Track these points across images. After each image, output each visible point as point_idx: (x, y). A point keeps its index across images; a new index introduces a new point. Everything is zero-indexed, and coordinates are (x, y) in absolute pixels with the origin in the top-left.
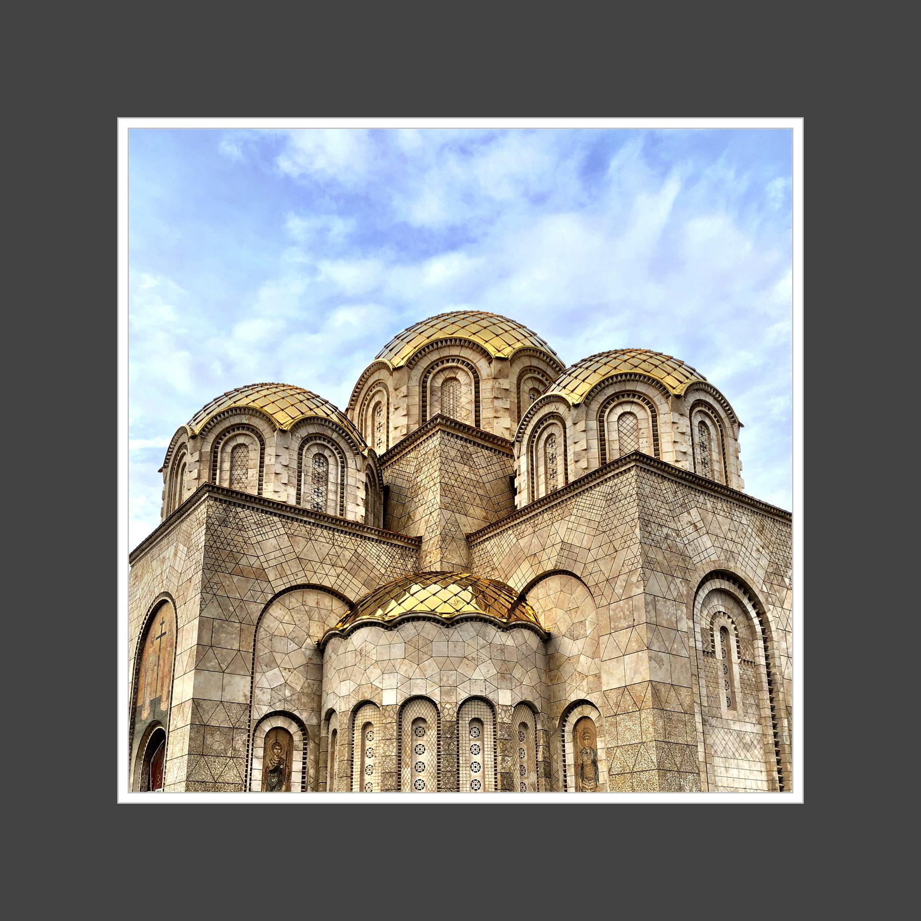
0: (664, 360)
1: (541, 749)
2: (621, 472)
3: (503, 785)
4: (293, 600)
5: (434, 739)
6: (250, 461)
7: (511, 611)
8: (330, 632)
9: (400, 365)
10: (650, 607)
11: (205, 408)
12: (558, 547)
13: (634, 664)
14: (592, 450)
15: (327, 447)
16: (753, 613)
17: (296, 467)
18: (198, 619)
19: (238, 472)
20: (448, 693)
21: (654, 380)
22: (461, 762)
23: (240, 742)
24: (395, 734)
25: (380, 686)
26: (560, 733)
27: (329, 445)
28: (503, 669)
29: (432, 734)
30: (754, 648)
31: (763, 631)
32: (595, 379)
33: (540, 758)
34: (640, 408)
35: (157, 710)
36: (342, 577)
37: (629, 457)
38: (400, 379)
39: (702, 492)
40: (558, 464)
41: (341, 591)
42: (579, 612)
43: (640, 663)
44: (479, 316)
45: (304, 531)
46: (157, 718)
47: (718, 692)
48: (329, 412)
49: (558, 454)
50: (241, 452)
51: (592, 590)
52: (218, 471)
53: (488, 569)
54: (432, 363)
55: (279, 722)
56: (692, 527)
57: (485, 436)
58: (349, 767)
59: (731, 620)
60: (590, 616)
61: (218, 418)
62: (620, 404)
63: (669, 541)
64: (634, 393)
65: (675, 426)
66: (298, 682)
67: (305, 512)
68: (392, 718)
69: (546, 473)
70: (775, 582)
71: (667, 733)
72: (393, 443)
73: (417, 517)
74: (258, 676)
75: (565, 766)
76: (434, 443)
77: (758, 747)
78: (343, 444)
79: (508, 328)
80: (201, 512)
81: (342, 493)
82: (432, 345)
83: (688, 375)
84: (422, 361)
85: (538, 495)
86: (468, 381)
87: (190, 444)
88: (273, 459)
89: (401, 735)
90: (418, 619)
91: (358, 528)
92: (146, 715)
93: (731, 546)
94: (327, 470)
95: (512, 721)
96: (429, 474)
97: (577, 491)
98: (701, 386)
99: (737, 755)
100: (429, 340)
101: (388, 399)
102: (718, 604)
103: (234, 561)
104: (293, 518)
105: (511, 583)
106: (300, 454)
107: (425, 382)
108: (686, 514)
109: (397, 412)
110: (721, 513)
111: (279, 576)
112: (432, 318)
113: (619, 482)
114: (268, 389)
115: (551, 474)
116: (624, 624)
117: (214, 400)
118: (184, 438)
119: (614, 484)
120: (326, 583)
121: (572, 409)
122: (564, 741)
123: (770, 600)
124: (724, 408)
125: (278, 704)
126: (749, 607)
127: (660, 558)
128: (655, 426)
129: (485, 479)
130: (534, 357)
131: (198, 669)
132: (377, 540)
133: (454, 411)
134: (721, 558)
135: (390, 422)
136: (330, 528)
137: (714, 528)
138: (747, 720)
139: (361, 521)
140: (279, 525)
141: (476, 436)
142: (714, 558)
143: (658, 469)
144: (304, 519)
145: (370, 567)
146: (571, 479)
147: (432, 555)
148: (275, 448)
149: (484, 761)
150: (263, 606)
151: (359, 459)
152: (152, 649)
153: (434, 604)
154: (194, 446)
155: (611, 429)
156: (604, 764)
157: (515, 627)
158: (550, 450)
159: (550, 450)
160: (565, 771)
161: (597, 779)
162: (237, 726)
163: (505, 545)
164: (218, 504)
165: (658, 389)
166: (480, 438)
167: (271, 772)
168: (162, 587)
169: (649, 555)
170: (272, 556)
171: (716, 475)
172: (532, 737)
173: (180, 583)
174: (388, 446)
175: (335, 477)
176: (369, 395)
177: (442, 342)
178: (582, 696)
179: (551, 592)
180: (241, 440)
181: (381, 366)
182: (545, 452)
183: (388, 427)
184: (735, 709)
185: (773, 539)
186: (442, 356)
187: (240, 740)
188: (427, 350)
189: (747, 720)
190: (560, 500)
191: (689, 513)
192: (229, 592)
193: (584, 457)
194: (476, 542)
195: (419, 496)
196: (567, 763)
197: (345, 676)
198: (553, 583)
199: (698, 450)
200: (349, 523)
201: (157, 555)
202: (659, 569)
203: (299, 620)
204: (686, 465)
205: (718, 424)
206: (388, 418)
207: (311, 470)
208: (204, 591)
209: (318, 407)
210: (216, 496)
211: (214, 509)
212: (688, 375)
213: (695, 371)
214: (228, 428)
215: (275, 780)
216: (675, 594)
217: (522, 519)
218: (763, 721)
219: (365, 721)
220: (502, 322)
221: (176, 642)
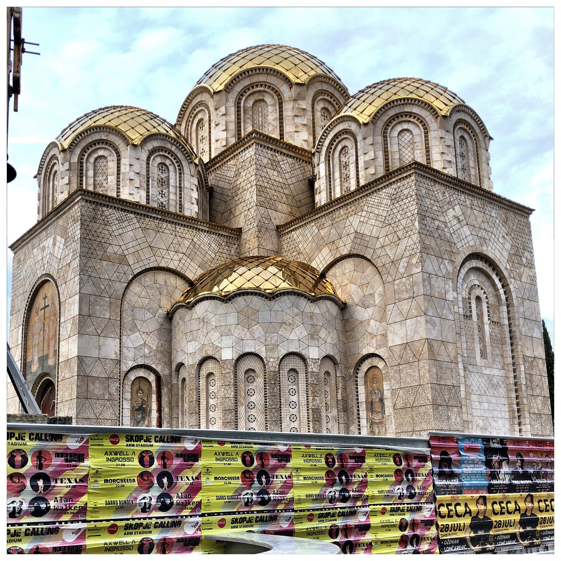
0: (433, 87)
1: (340, 391)
2: (403, 178)
3: (314, 418)
4: (148, 279)
5: (262, 385)
6: (109, 170)
7: (315, 286)
8: (178, 304)
9: (218, 90)
10: (427, 282)
11: (71, 126)
12: (352, 236)
13: (414, 326)
14: (378, 160)
15: (167, 157)
16: (499, 285)
17: (145, 174)
18: (78, 295)
19: (100, 178)
20: (272, 350)
21: (426, 104)
22: (282, 401)
23: (114, 388)
24: (232, 381)
25: (219, 345)
26: (354, 379)
27: (169, 156)
28: (312, 331)
29: (260, 381)
30: (500, 313)
31: (507, 299)
32: (379, 103)
33: (340, 398)
34: (415, 126)
35: (45, 365)
36: (183, 261)
37: (410, 165)
38: (219, 101)
39: (463, 192)
40: (351, 170)
41: (182, 272)
42: (369, 287)
43: (419, 325)
44: (280, 49)
45: (153, 225)
46: (45, 371)
47: (474, 346)
48: (168, 130)
49: (351, 162)
50: (102, 162)
51: (380, 270)
52: (84, 178)
53: (295, 254)
54: (244, 87)
55: (141, 373)
56: (456, 220)
57: (290, 147)
58: (197, 406)
59: (483, 291)
60: (378, 290)
61: (83, 135)
62: (400, 123)
63: (439, 231)
64: (410, 114)
65: (443, 140)
66: (154, 342)
67: (153, 210)
68: (229, 369)
69: (341, 177)
70: (516, 261)
71: (439, 378)
72: (215, 152)
73: (237, 213)
74: (124, 338)
75: (358, 403)
76: (250, 152)
77: (502, 386)
78: (180, 155)
79: (303, 59)
80: (76, 210)
81: (180, 194)
82: (244, 73)
83: (452, 99)
84: (237, 86)
85: (335, 195)
86: (273, 102)
87: (60, 157)
88: (128, 168)
89: (236, 382)
90: (248, 294)
91: (193, 222)
92: (35, 368)
93: (484, 234)
94: (169, 176)
95: (319, 370)
96: (246, 178)
97: (367, 192)
98: (461, 108)
99: (487, 392)
100: (241, 70)
101: (210, 117)
102: (474, 279)
103: (102, 250)
104: (145, 215)
105: (314, 265)
106: (148, 164)
107: (239, 103)
108: (451, 210)
109: (218, 128)
110: (477, 209)
111: (136, 261)
112: (242, 50)
113: (401, 185)
114: (119, 111)
115: (345, 178)
116: (405, 295)
117: (77, 120)
118: (55, 151)
119: (397, 187)
120: (172, 266)
121: (362, 126)
122: (357, 385)
123: (512, 275)
124: (478, 125)
125: (140, 359)
126: (497, 281)
127: (433, 244)
128: (427, 140)
129: (290, 181)
130: (324, 82)
131: (80, 334)
132: (208, 231)
133: (262, 126)
134: (477, 244)
135: (212, 135)
136: (173, 222)
137: (471, 220)
138: (495, 366)
139: (195, 216)
140: (135, 221)
141: (282, 147)
142: (472, 243)
143: (431, 174)
144: (154, 215)
145: (204, 253)
146: (362, 183)
147: (250, 242)
148: (128, 160)
149: (299, 400)
150: (126, 284)
151: (192, 167)
152: (37, 318)
153: (257, 282)
154: (64, 158)
155: (393, 142)
156: (389, 401)
157: (320, 299)
158: (344, 159)
159: (344, 159)
160: (358, 407)
161: (383, 412)
162: (111, 376)
163: (309, 235)
164: (89, 204)
165: (429, 111)
166: (285, 148)
167: (137, 410)
168: (44, 269)
169: (425, 242)
170: (130, 245)
171: (473, 178)
172: (334, 382)
173: (60, 267)
174: (210, 155)
175: (174, 181)
176: (193, 114)
177: (252, 71)
178: (372, 350)
179: (347, 271)
180: (101, 153)
181: (204, 90)
182: (340, 161)
183: (210, 140)
184: (486, 358)
185: (514, 227)
186: (252, 82)
187: (114, 387)
188: (240, 77)
189: (495, 366)
190: (353, 199)
191: (454, 209)
192: (100, 274)
193: (372, 165)
194: (284, 232)
195: (239, 196)
196: (360, 401)
197: (191, 338)
198: (348, 265)
199: (459, 160)
200: (187, 218)
201: (37, 245)
202: (432, 253)
203: (153, 295)
204: (451, 171)
205: (474, 138)
206: (210, 132)
207: (156, 176)
208: (81, 273)
209: (159, 125)
210: (87, 198)
211: (86, 208)
212: (452, 99)
213: (456, 95)
214: (90, 143)
215: (140, 416)
216: (444, 272)
217: (322, 214)
218: (506, 367)
219: (208, 372)
220: (299, 54)
221: (60, 313)
